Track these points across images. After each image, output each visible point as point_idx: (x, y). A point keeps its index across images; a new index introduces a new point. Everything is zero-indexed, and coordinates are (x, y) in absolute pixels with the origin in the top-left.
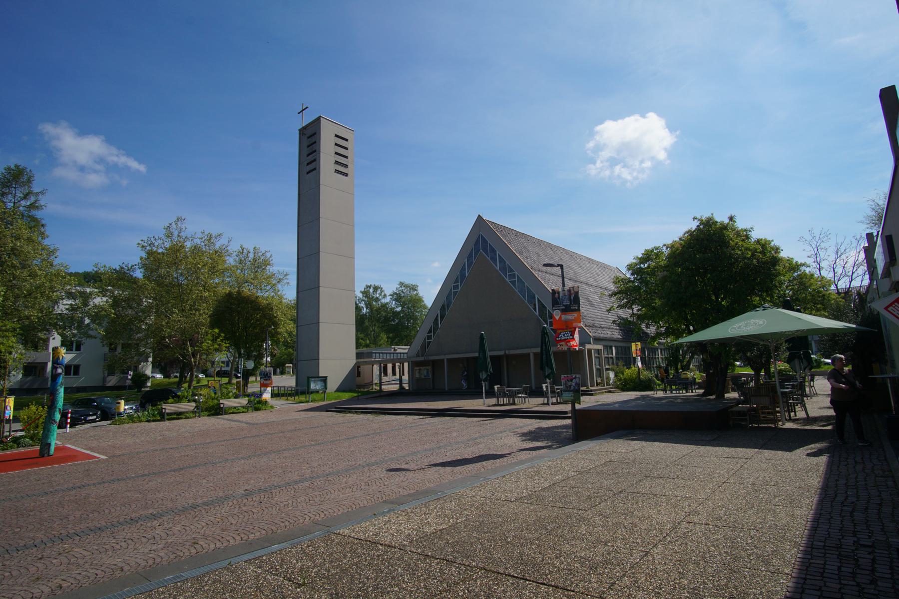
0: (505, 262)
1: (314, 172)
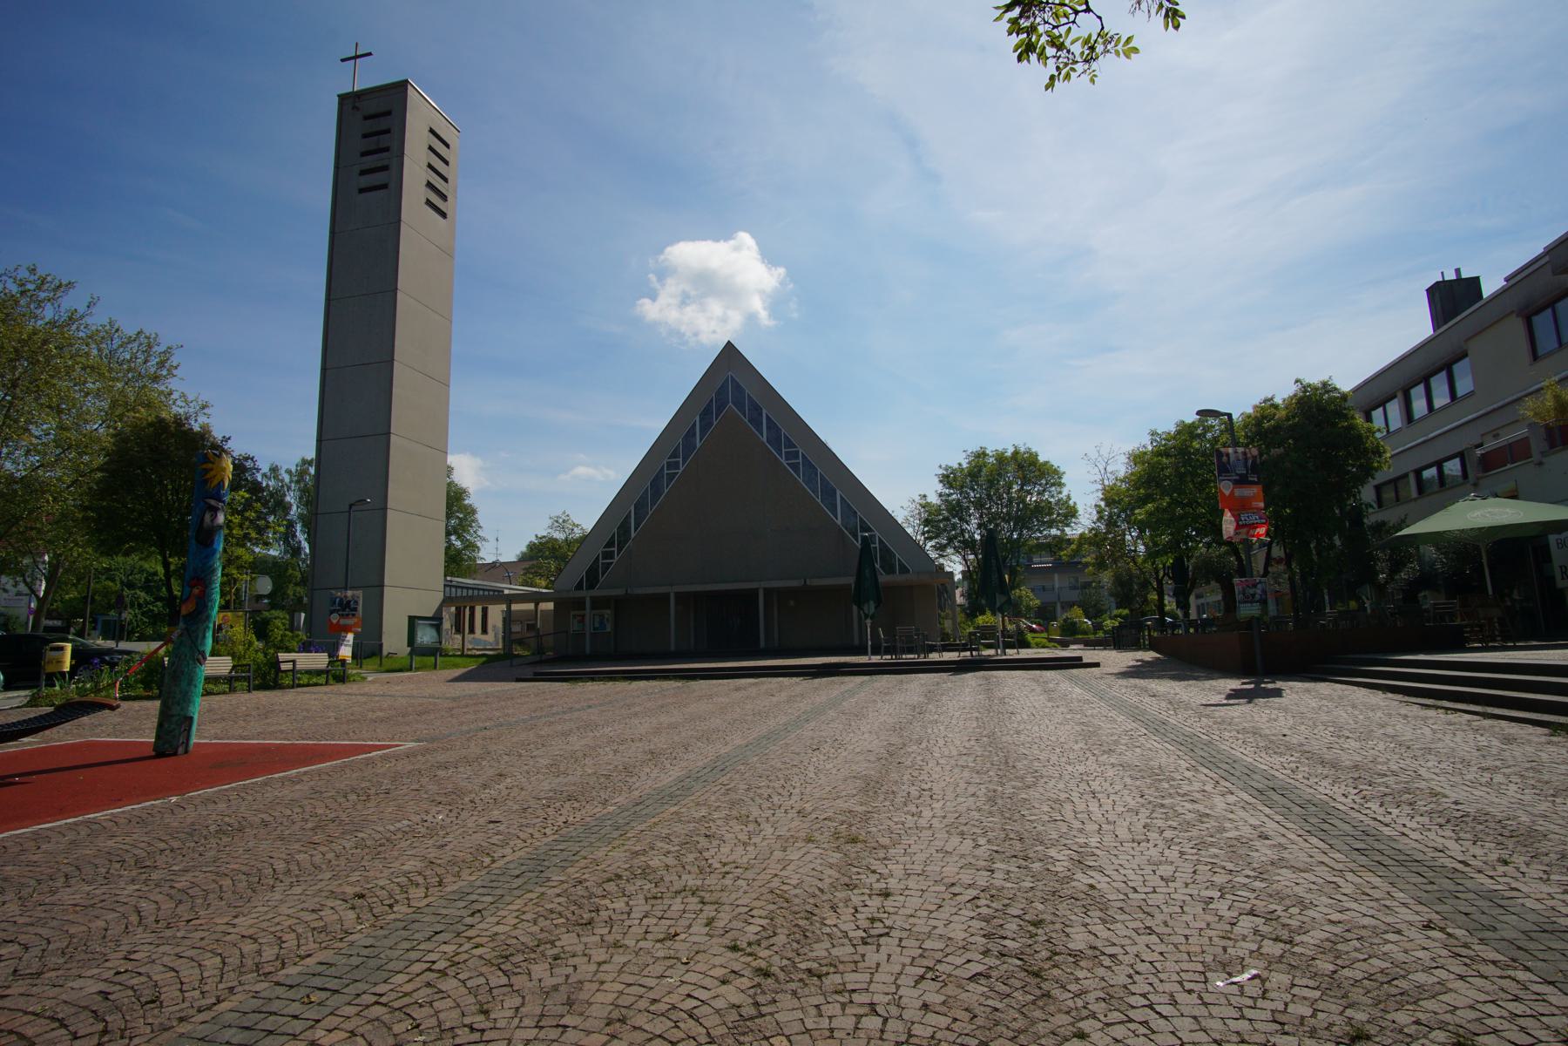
1: (381, 193)
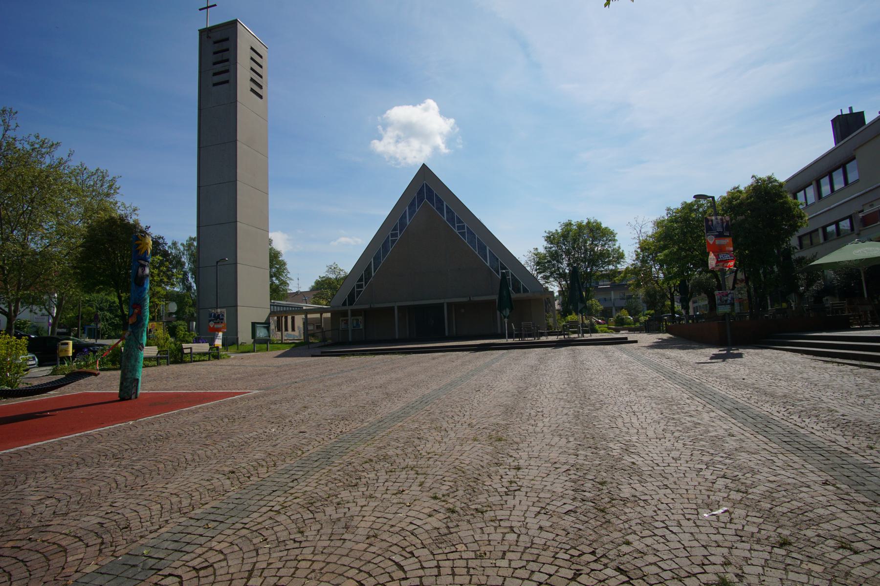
0: (453, 213)
1: (226, 86)
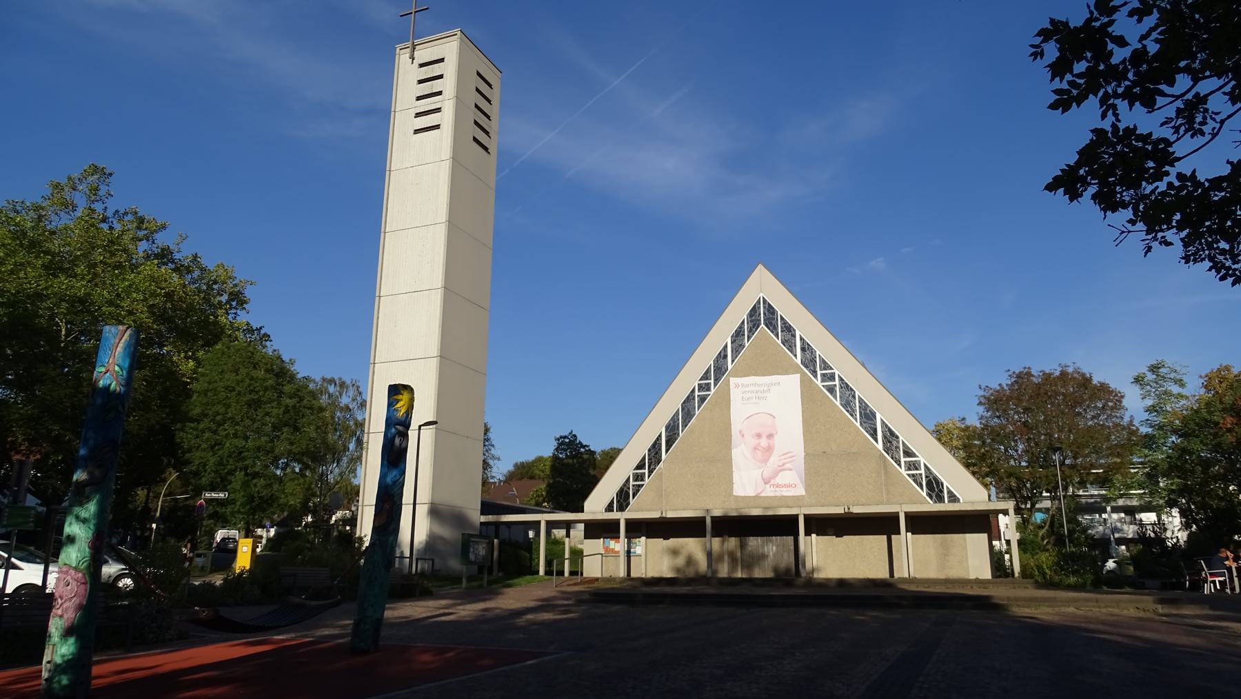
0: (813, 352)
